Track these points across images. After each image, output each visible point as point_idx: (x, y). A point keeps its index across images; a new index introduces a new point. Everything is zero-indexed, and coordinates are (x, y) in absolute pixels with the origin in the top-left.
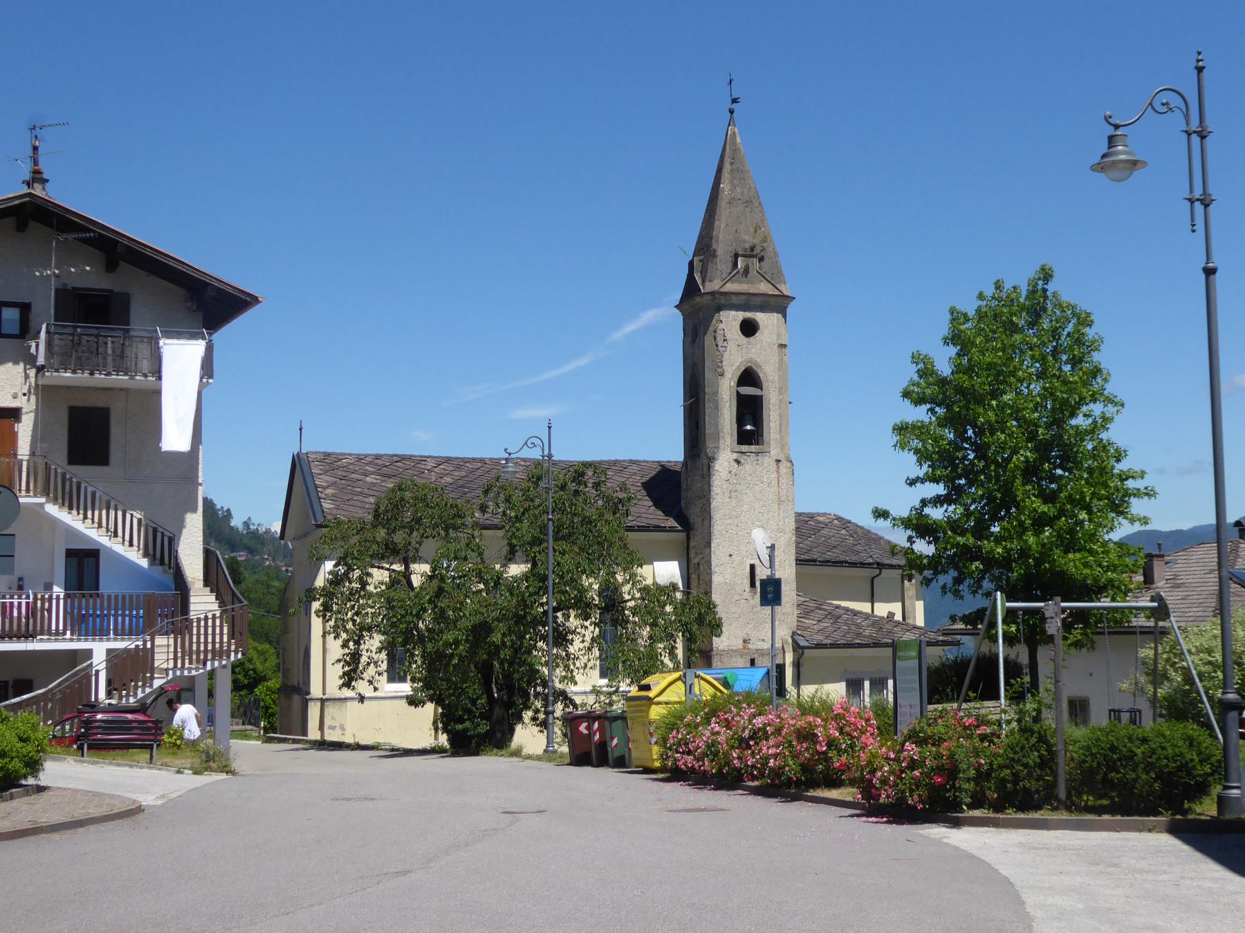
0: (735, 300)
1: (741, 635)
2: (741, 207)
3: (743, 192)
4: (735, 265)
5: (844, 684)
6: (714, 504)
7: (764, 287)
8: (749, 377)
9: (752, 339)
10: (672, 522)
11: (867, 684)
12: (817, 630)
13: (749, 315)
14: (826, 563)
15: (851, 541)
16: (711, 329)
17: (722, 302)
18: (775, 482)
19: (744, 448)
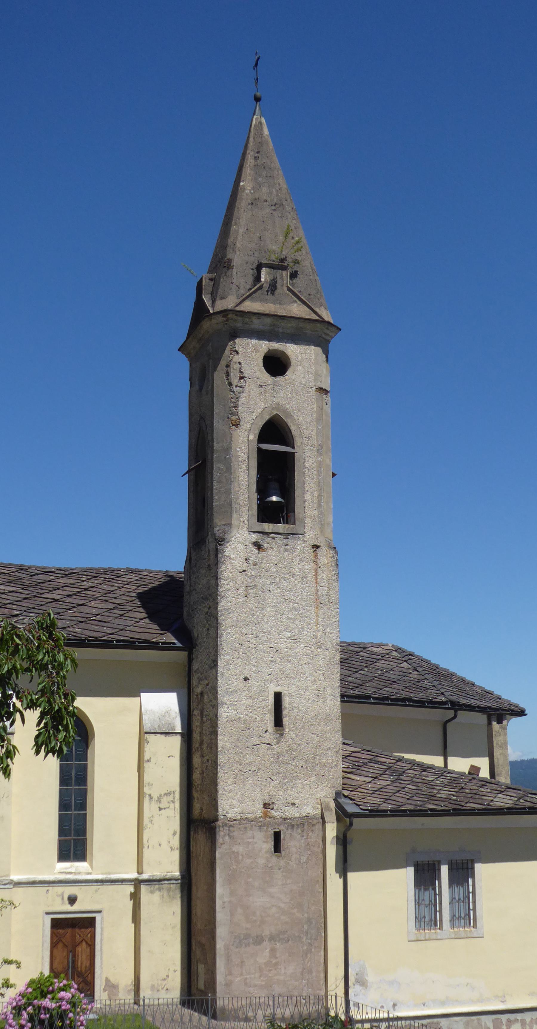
0: (256, 324)
1: (260, 797)
2: (268, 210)
3: (270, 193)
4: (258, 278)
5: (410, 871)
6: (223, 604)
7: (297, 310)
8: (275, 430)
9: (280, 379)
10: (169, 637)
11: (445, 870)
12: (372, 789)
13: (275, 345)
14: (384, 700)
15: (415, 675)
16: (223, 363)
17: (239, 325)
18: (311, 577)
19: (268, 527)
